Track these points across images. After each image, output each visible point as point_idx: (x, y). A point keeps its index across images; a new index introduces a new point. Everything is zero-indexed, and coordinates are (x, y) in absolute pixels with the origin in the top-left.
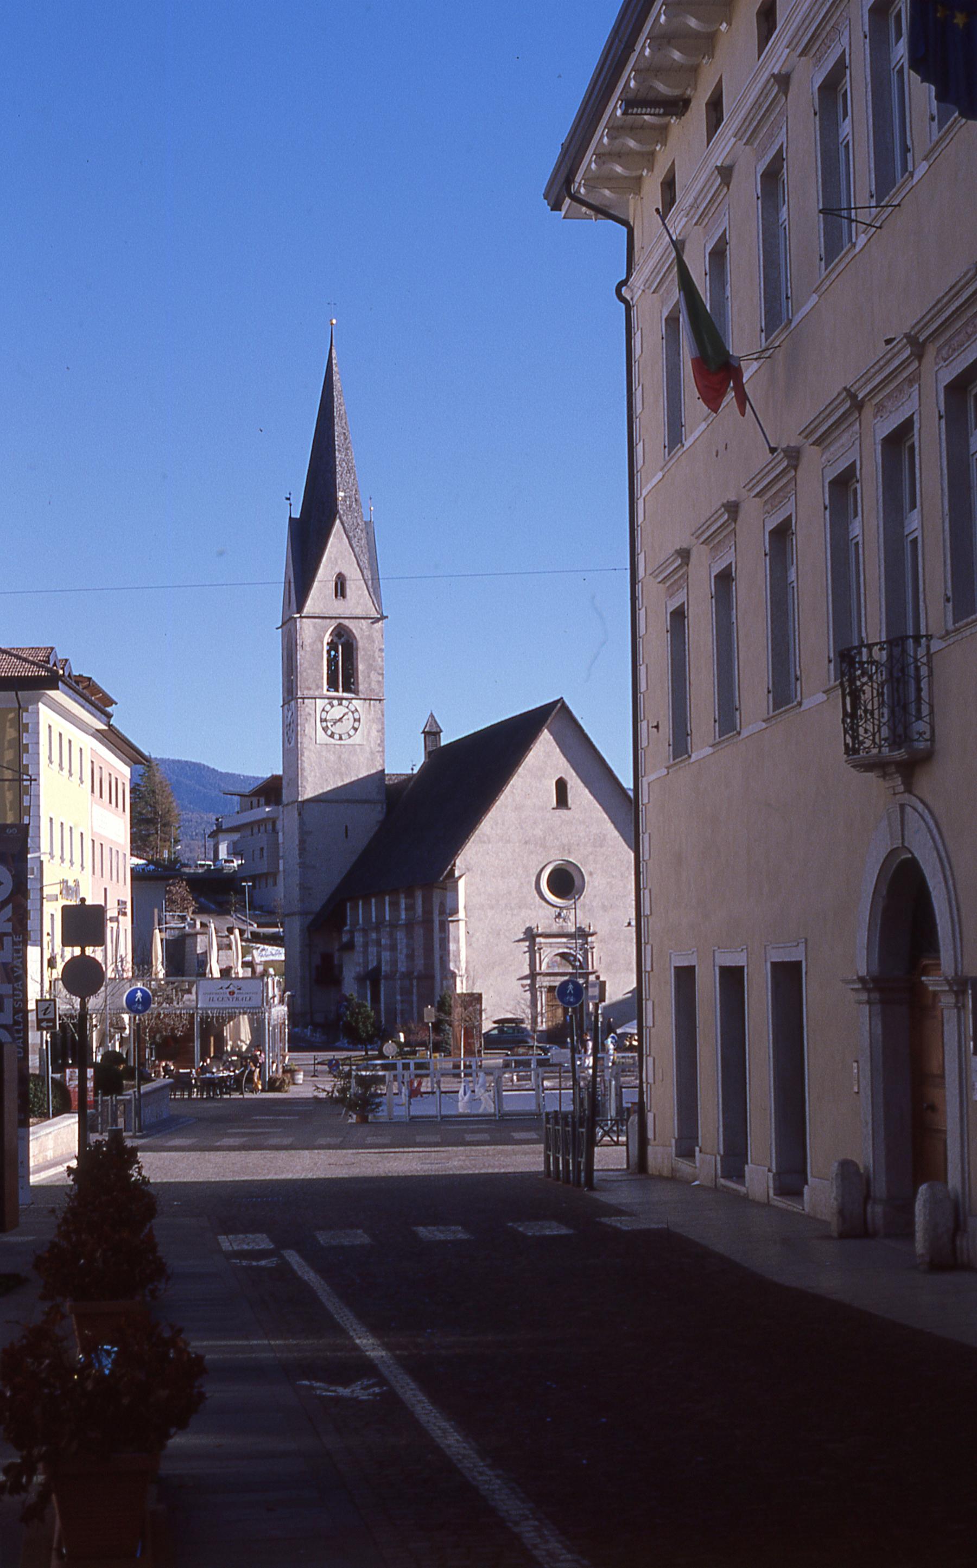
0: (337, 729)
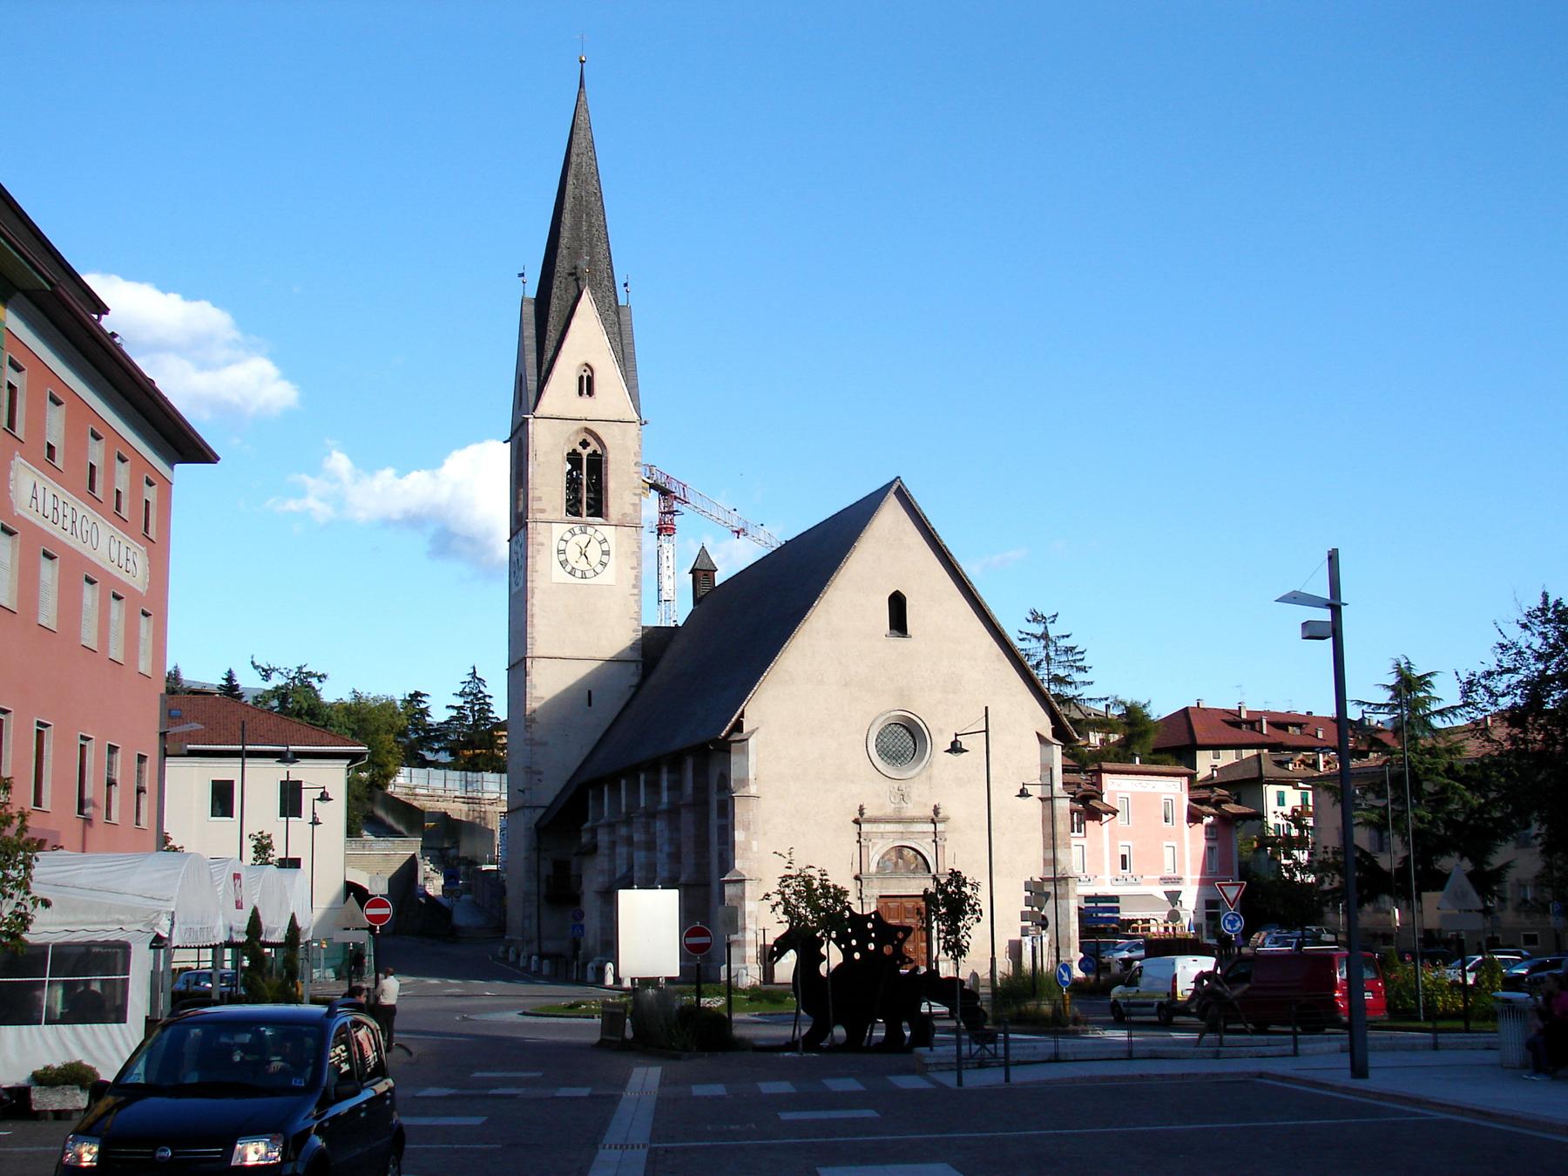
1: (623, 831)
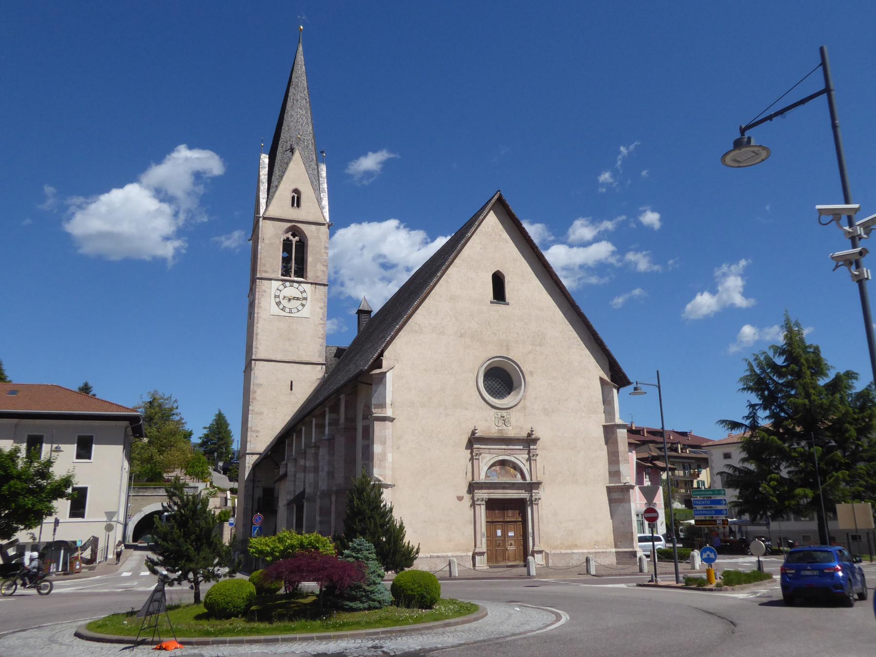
0: (285, 303)
1: (302, 462)
